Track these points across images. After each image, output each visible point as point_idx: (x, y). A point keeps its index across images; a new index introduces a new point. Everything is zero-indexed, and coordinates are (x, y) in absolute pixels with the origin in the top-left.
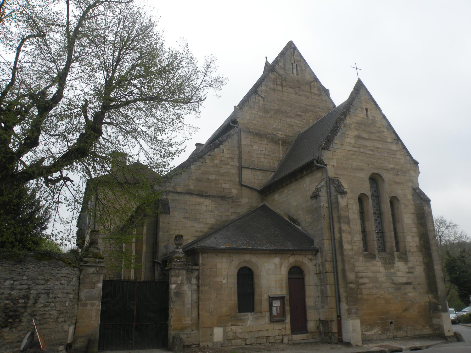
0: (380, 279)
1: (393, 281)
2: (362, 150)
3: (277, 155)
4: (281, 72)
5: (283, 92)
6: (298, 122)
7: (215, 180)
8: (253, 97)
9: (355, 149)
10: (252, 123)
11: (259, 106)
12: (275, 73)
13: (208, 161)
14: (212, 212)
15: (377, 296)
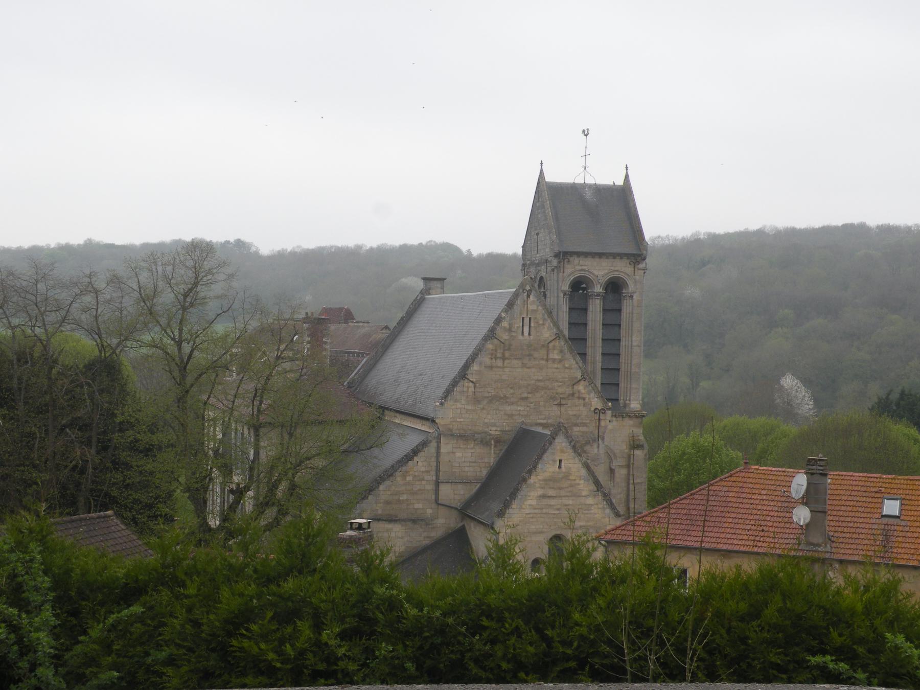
2: (544, 511)
3: (486, 460)
4: (505, 336)
5: (503, 367)
6: (522, 409)
7: (407, 500)
8: (461, 384)
9: (536, 511)
11: (467, 397)
13: (399, 479)
14: (402, 538)
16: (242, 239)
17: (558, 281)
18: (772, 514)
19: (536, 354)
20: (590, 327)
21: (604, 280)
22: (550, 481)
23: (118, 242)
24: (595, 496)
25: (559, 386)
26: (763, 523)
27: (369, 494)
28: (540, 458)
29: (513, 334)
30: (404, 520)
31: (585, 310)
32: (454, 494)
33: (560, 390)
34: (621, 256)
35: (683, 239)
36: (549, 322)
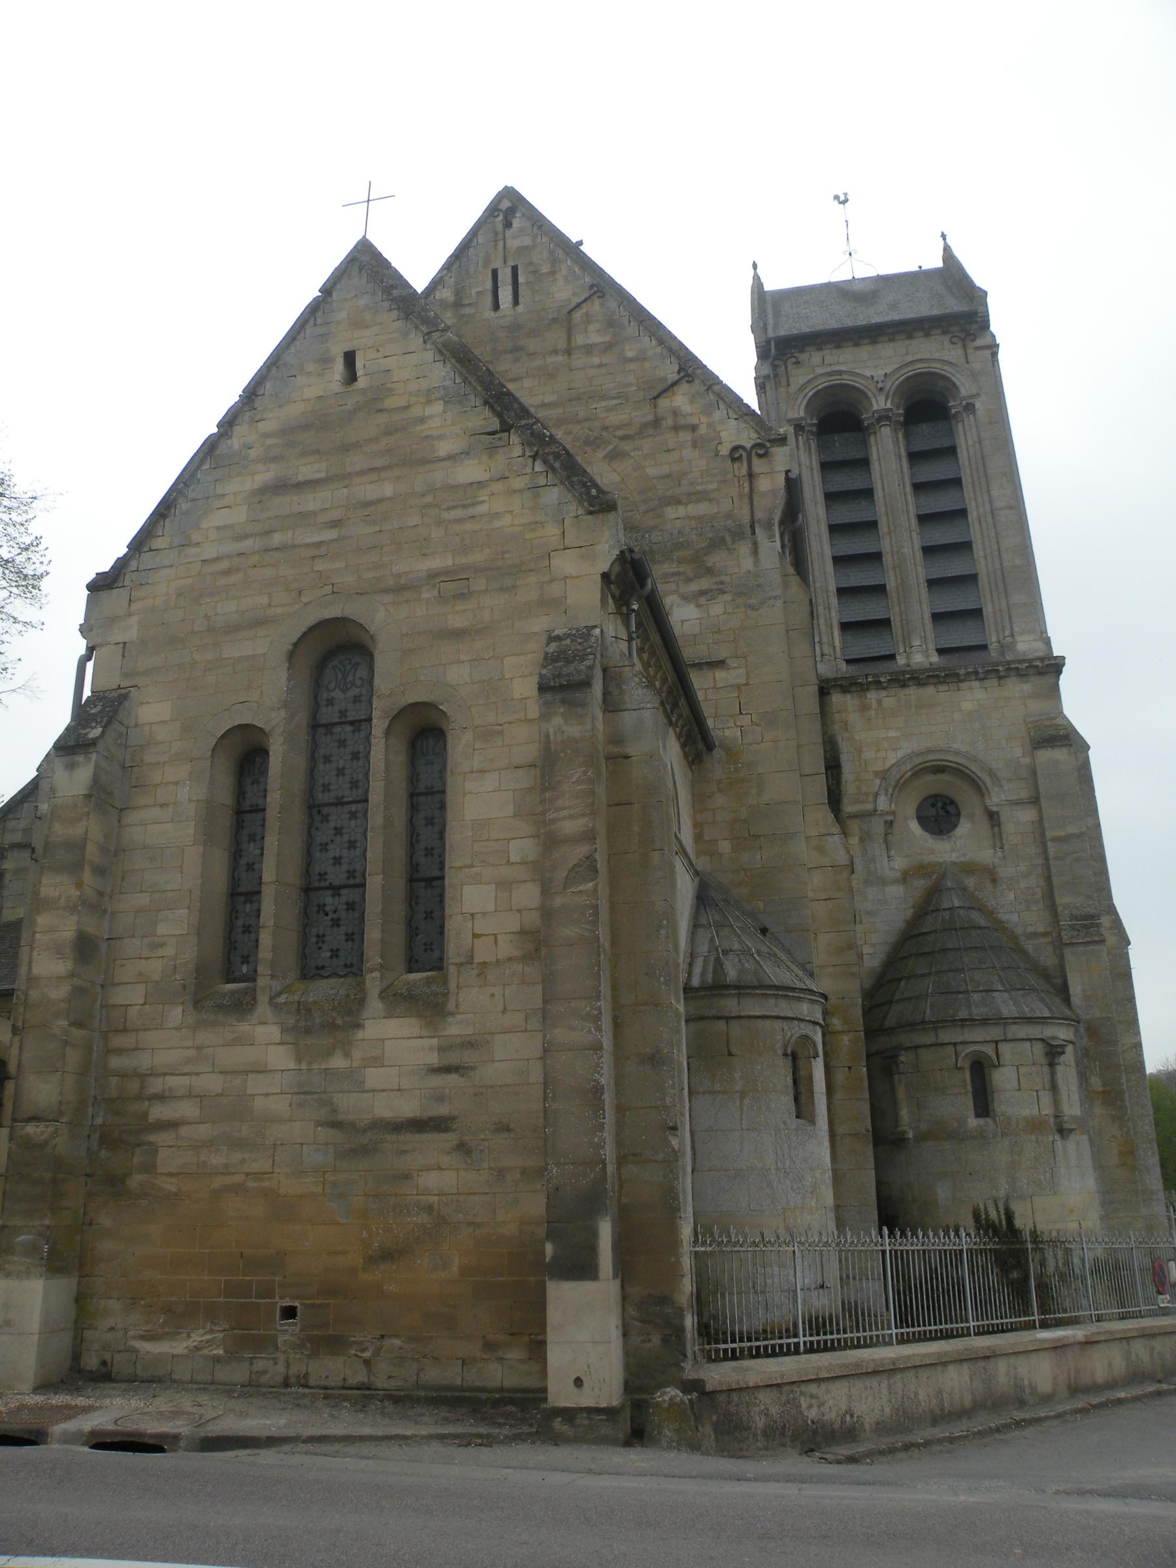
0: (259, 1103)
1: (335, 1111)
2: (277, 539)
15: (228, 1180)
21: (891, 384)
25: (610, 410)
29: (467, 310)
33: (615, 419)
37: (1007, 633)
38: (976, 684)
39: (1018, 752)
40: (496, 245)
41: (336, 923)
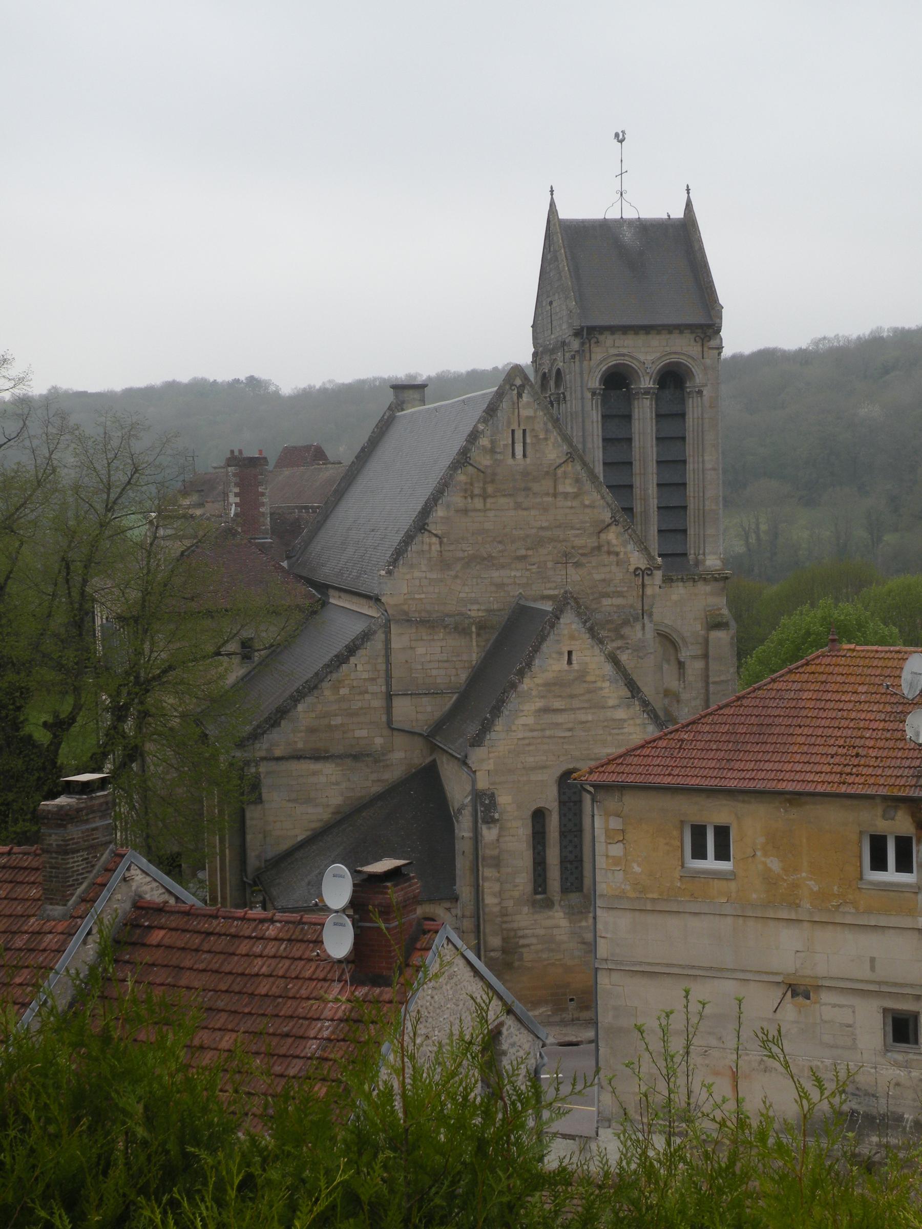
2: (548, 733)
3: (465, 658)
4: (485, 461)
5: (485, 511)
6: (518, 574)
8: (419, 538)
9: (535, 734)
10: (414, 599)
11: (430, 559)
12: (470, 468)
13: (327, 693)
14: (337, 784)
16: (256, 375)
17: (581, 373)
18: (874, 725)
19: (536, 487)
20: (636, 443)
21: (655, 368)
22: (554, 686)
23: (92, 389)
24: (628, 706)
25: (576, 536)
26: (858, 742)
27: (282, 718)
28: (537, 649)
29: (499, 457)
30: (340, 757)
31: (628, 418)
32: (413, 712)
33: (578, 542)
34: (680, 328)
35: (859, 338)
36: (554, 435)
37: (701, 552)
38: (681, 584)
39: (699, 627)
40: (513, 412)
41: (572, 873)
